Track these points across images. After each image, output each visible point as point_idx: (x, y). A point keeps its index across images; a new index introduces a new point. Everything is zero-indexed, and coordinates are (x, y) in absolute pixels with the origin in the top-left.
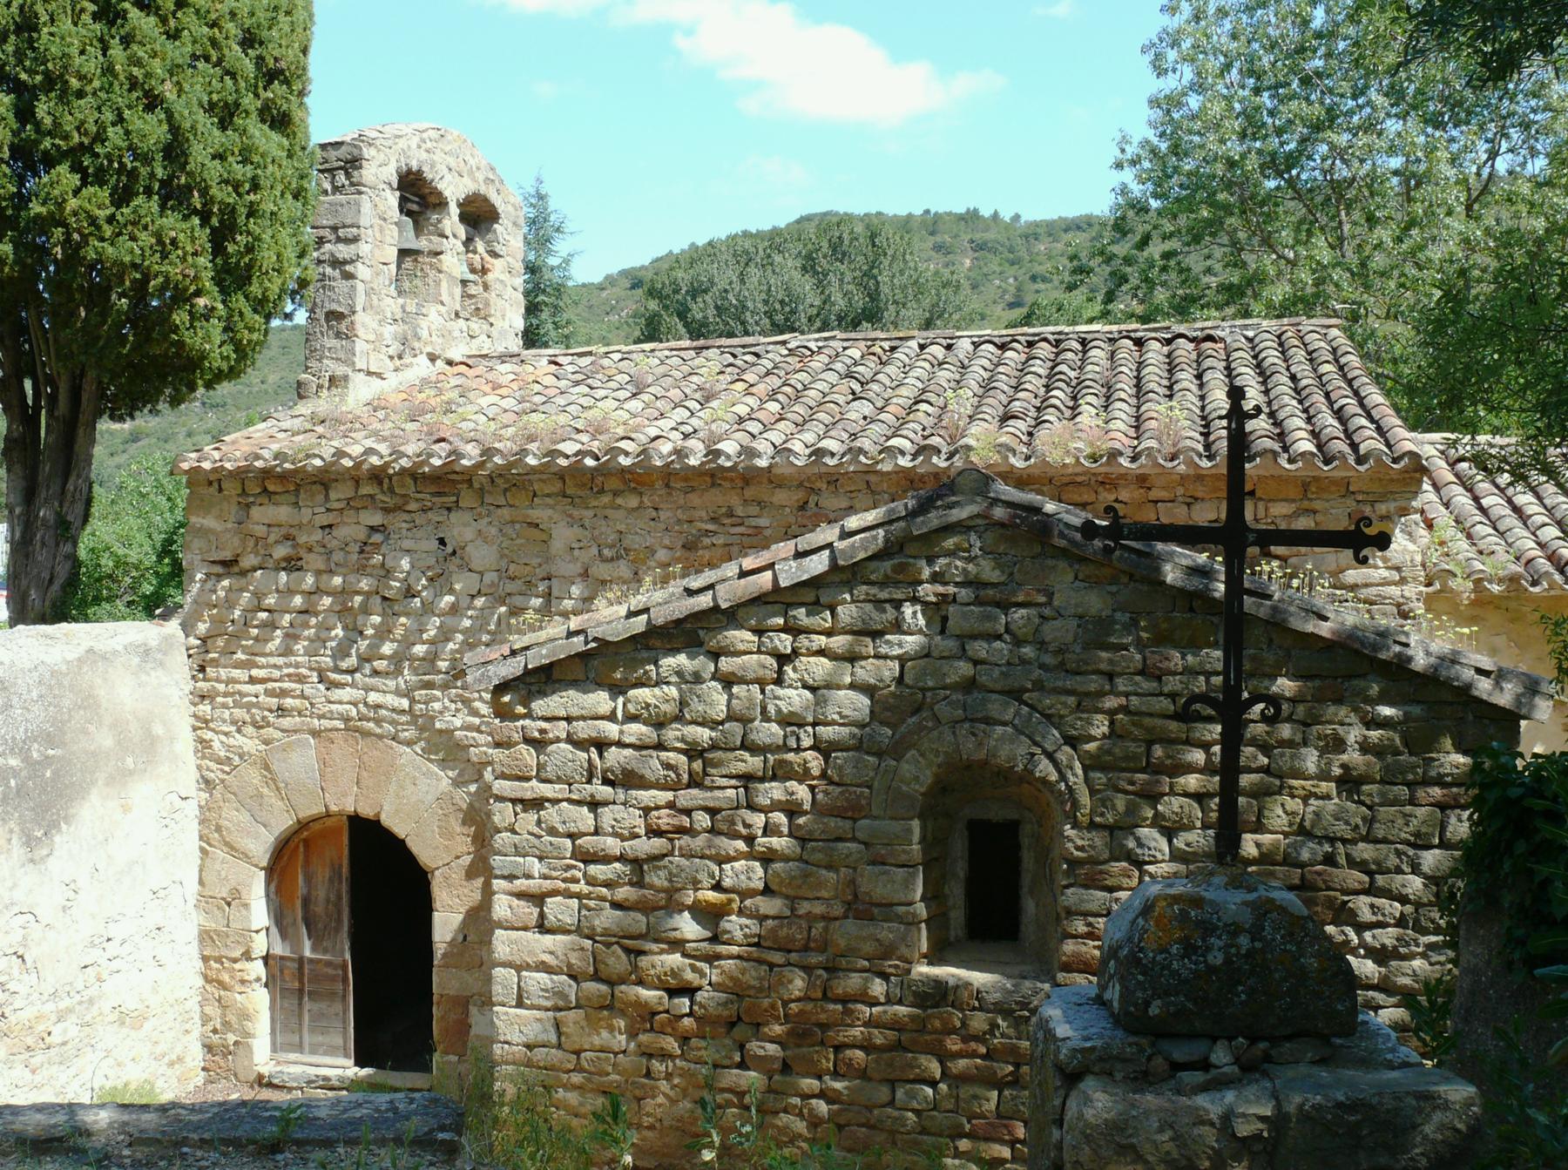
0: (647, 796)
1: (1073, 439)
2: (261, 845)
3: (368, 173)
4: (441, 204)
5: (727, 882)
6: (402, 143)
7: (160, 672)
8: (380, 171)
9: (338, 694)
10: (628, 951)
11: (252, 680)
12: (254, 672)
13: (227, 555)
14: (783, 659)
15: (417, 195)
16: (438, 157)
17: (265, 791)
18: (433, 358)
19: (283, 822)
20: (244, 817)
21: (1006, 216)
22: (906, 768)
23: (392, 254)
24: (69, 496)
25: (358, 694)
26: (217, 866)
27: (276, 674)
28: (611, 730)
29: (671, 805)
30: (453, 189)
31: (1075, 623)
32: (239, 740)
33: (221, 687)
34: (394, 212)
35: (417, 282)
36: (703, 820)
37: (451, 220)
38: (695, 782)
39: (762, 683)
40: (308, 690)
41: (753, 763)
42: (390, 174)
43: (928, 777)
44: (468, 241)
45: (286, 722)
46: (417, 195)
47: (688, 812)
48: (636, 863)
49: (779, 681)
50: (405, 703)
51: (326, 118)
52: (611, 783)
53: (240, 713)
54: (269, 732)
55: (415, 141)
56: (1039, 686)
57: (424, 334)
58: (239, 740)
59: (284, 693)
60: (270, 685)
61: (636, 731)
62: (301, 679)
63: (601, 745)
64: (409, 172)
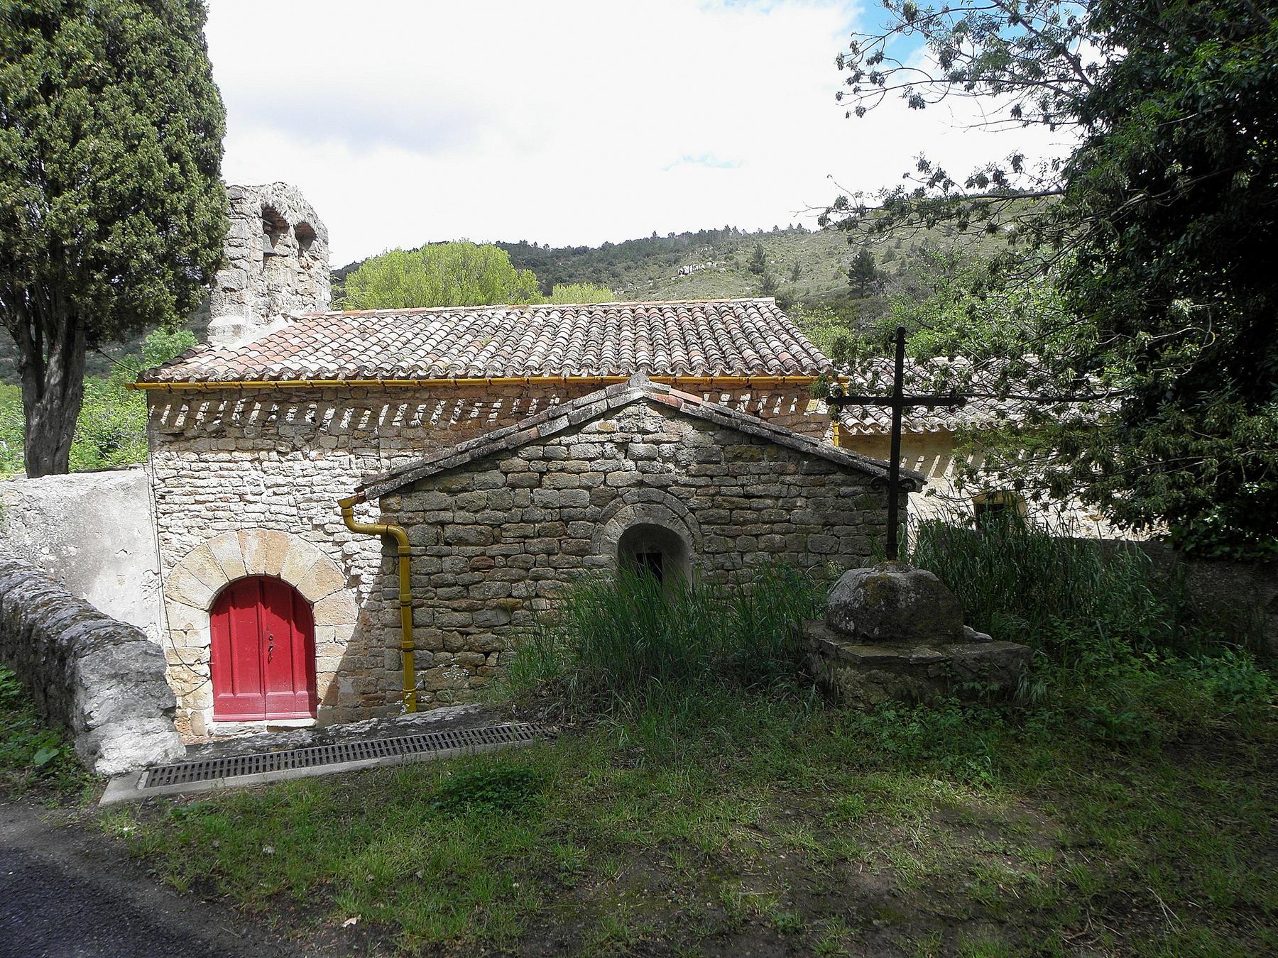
0: (469, 549)
2: (205, 597)
3: (246, 207)
4: (285, 228)
5: (515, 593)
6: (263, 190)
7: (137, 501)
8: (252, 206)
9: (251, 507)
10: (461, 633)
11: (197, 502)
12: (198, 498)
14: (542, 474)
15: (273, 222)
16: (283, 199)
17: (207, 566)
18: (285, 316)
19: (219, 582)
20: (194, 581)
21: (541, 245)
23: (260, 256)
24: (68, 399)
26: (177, 612)
27: (212, 498)
28: (447, 516)
29: (483, 554)
30: (292, 219)
31: (693, 450)
32: (187, 538)
33: (176, 507)
34: (261, 231)
35: (273, 272)
36: (501, 561)
37: (291, 238)
38: (496, 542)
39: (532, 488)
40: (233, 507)
41: (530, 529)
42: (257, 207)
43: (620, 532)
44: (300, 250)
45: (219, 526)
46: (273, 222)
47: (493, 557)
48: (466, 586)
49: (540, 486)
51: (232, 171)
52: (450, 545)
53: (187, 522)
54: (210, 532)
55: (271, 189)
57: (280, 303)
59: (217, 509)
60: (208, 505)
61: (462, 516)
63: (443, 524)
64: (268, 207)
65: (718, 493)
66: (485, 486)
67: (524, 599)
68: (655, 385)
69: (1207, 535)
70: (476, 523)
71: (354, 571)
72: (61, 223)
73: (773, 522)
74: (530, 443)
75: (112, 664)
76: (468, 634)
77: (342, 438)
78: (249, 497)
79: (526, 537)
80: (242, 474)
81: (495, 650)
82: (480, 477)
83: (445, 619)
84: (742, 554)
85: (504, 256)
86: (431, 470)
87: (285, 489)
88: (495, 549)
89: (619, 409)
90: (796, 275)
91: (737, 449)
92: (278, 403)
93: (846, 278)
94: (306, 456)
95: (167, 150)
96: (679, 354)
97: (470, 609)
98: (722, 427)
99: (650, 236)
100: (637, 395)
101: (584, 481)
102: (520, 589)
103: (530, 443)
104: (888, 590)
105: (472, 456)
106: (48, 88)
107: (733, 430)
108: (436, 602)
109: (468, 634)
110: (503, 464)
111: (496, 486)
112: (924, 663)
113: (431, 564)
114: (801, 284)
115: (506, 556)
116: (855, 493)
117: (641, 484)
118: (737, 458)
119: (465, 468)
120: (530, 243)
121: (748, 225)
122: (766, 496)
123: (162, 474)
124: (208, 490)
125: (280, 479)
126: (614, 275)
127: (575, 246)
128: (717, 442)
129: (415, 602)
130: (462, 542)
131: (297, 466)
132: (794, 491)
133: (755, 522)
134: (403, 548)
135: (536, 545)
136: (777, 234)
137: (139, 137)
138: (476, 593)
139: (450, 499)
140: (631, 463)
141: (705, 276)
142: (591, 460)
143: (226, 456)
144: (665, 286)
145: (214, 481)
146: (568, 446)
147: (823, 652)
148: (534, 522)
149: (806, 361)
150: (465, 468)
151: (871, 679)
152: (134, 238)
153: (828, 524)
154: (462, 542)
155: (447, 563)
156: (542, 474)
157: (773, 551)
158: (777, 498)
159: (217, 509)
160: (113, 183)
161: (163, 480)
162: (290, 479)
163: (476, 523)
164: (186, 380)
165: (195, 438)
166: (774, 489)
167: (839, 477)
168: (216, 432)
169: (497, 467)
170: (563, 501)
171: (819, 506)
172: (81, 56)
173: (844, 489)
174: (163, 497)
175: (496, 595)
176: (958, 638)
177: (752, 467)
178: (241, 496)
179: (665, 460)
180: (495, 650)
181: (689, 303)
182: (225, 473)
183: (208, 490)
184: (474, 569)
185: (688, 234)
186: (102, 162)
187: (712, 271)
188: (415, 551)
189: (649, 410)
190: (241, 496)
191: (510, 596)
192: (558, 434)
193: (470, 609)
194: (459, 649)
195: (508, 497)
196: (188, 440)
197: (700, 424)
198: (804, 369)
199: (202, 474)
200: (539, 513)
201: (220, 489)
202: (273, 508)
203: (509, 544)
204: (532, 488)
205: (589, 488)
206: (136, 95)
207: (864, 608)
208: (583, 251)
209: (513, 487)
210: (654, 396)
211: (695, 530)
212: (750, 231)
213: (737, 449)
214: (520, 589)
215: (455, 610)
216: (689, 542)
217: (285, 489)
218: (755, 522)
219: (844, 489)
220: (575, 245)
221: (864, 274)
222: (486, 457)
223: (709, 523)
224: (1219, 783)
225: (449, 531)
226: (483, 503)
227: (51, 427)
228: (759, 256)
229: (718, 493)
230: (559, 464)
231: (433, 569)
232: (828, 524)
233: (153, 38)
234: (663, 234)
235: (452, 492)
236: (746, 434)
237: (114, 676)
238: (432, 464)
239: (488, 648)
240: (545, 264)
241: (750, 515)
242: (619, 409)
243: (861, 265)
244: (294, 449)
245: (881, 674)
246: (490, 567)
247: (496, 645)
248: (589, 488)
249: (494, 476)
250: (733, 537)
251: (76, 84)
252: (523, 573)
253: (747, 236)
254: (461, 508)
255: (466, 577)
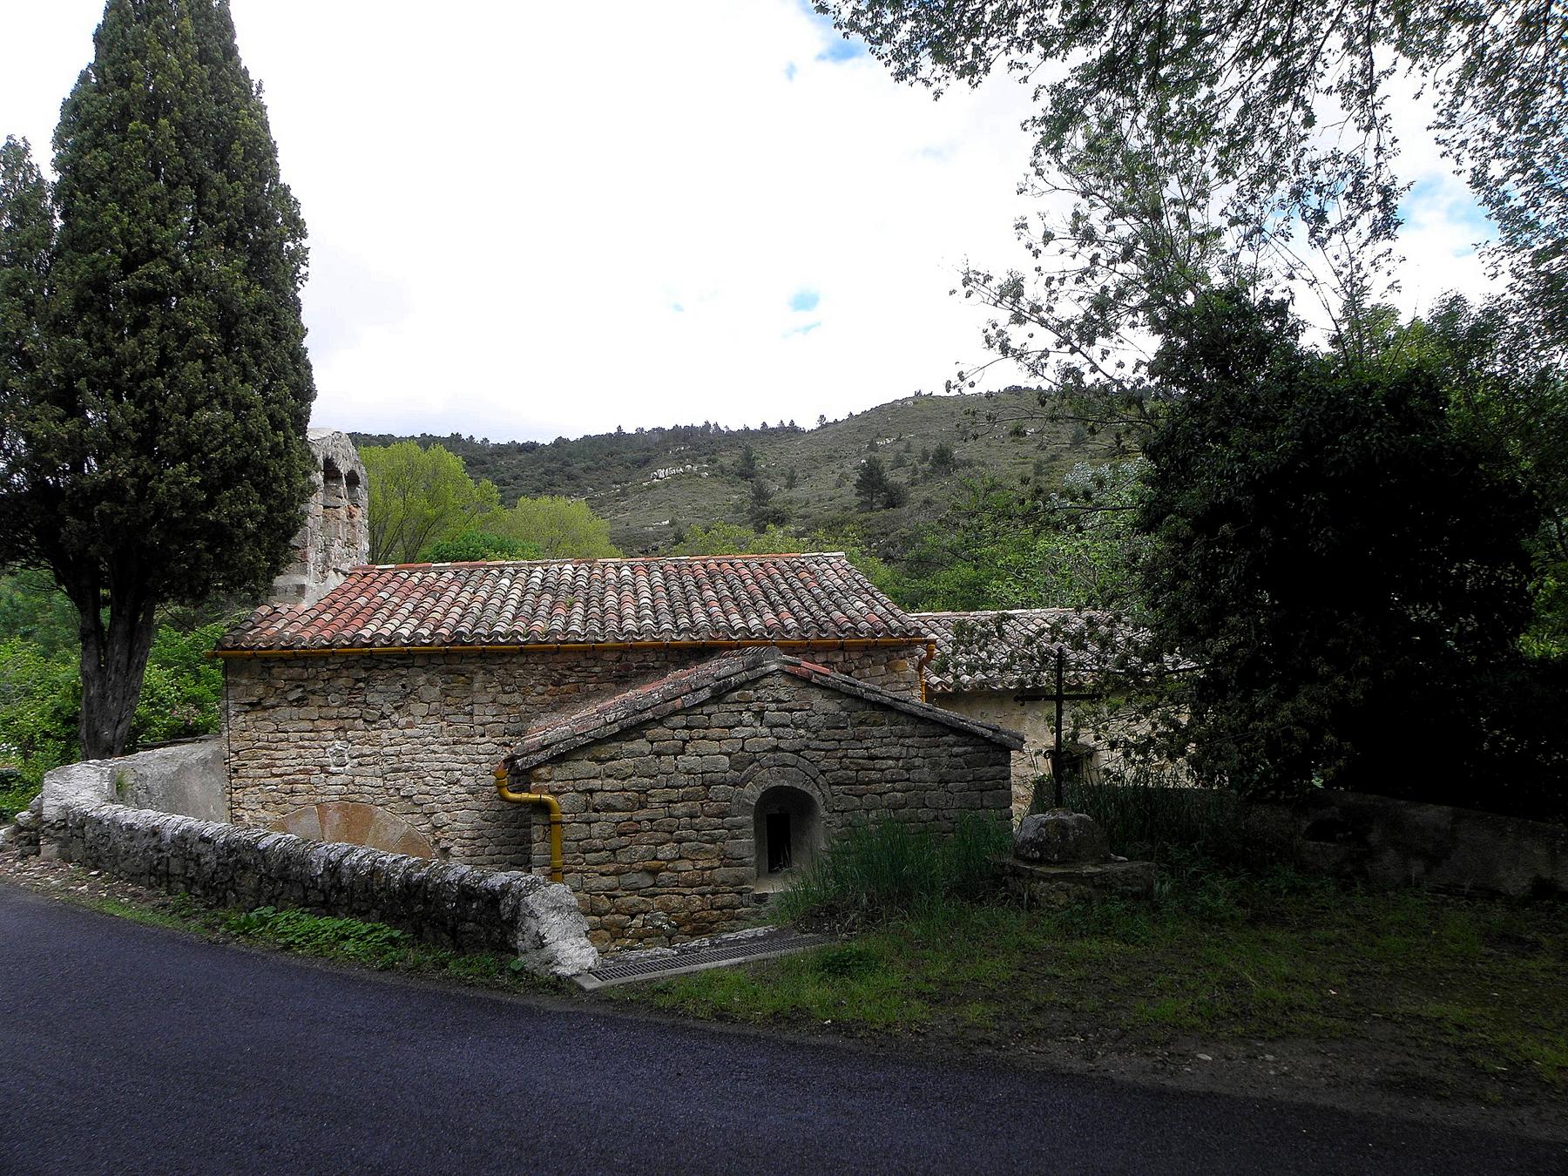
1: (561, 502)
5: (660, 856)
10: (608, 897)
13: (255, 700)
14: (685, 742)
16: (340, 449)
18: (336, 571)
22: (747, 790)
25: (347, 779)
27: (291, 770)
28: (597, 783)
29: (630, 819)
36: (646, 825)
38: (642, 807)
39: (676, 755)
41: (674, 794)
43: (758, 794)
48: (613, 851)
49: (683, 753)
50: (380, 782)
53: (262, 797)
56: (807, 747)
58: (263, 814)
59: (296, 782)
61: (610, 783)
62: (308, 772)
63: (591, 792)
65: (845, 756)
66: (632, 754)
67: (669, 861)
68: (789, 658)
69: (1259, 783)
70: (624, 790)
71: (443, 844)
72: (173, 496)
73: (894, 781)
74: (675, 713)
75: (552, 899)
76: (615, 897)
77: (434, 705)
78: (333, 769)
79: (670, 802)
80: (324, 744)
81: (641, 912)
82: (627, 746)
83: (594, 884)
84: (868, 811)
85: (454, 462)
86: (582, 741)
87: (371, 760)
88: (642, 814)
89: (756, 681)
90: (791, 483)
91: (862, 715)
92: (366, 670)
93: (850, 486)
94: (395, 725)
95: (271, 417)
96: (769, 616)
97: (617, 873)
98: (848, 695)
99: (613, 431)
100: (774, 667)
101: (725, 748)
102: (667, 851)
103: (675, 713)
104: (1061, 826)
105: (621, 726)
106: (165, 361)
107: (859, 698)
108: (584, 867)
109: (615, 897)
110: (649, 733)
111: (642, 754)
112: (1091, 876)
113: (579, 831)
114: (800, 492)
115: (651, 821)
116: (966, 753)
117: (776, 749)
118: (861, 723)
119: (614, 737)
120: (465, 437)
121: (732, 421)
122: (889, 758)
123: (235, 746)
124: (287, 762)
125: (367, 750)
126: (570, 477)
127: (521, 441)
128: (844, 709)
129: (565, 868)
130: (609, 808)
131: (385, 735)
132: (913, 752)
133: (879, 782)
134: (555, 816)
135: (680, 808)
136: (765, 431)
137: (248, 408)
138: (622, 857)
139: (599, 768)
140: (767, 730)
141: (684, 482)
142: (730, 728)
143: (307, 725)
144: (636, 492)
145: (294, 752)
146: (709, 715)
147: (1017, 873)
148: (678, 787)
149: (894, 623)
150: (614, 737)
151: (1060, 888)
152: (240, 507)
153: (943, 781)
154: (609, 808)
155: (596, 829)
156: (685, 742)
157: (896, 807)
158: (898, 759)
159: (296, 782)
160: (224, 453)
161: (237, 753)
162: (377, 749)
163: (624, 790)
164: (270, 648)
165: (273, 707)
166: (895, 751)
167: (951, 738)
168: (297, 700)
169: (644, 736)
170: (705, 768)
171: (935, 765)
172: (198, 330)
173: (955, 750)
174: (236, 771)
175: (642, 858)
176: (1107, 860)
177: (875, 731)
178: (323, 769)
179: (797, 727)
180: (641, 912)
181: (767, 559)
182: (307, 743)
183: (287, 762)
184: (621, 834)
185: (660, 430)
186: (215, 434)
187: (690, 475)
188: (565, 818)
189: (782, 680)
190: (323, 769)
191: (655, 858)
192: (701, 704)
193: (617, 873)
194: (607, 912)
195: (655, 764)
196: (265, 709)
197: (827, 693)
198: (894, 631)
199: (280, 745)
200: (682, 779)
201: (299, 761)
202: (357, 780)
203: (656, 809)
204: (676, 755)
205: (729, 754)
206: (244, 365)
207: (1047, 841)
208: (531, 447)
209: (659, 754)
210: (787, 668)
211: (826, 790)
212: (734, 428)
213: (862, 715)
214: (667, 851)
215: (602, 874)
216: (820, 802)
217: (371, 760)
218: (879, 782)
219: (955, 750)
220: (521, 440)
221: (873, 485)
222: (632, 727)
223: (838, 784)
224: (1278, 936)
225: (598, 798)
226: (630, 771)
227: (115, 699)
228: (749, 460)
229: (845, 756)
230: (702, 732)
231: (582, 835)
232: (943, 781)
233: (260, 309)
234: (629, 429)
235: (600, 761)
236: (869, 701)
237: (554, 908)
238: (583, 735)
239: (635, 910)
240: (484, 463)
241: (875, 775)
242: (756, 681)
243: (870, 475)
244: (383, 716)
245: (1066, 885)
246: (637, 832)
247: (642, 906)
248: (729, 754)
249: (640, 745)
250: (860, 796)
251: (193, 356)
252: (667, 836)
253: (730, 434)
254: (610, 776)
255: (614, 842)
